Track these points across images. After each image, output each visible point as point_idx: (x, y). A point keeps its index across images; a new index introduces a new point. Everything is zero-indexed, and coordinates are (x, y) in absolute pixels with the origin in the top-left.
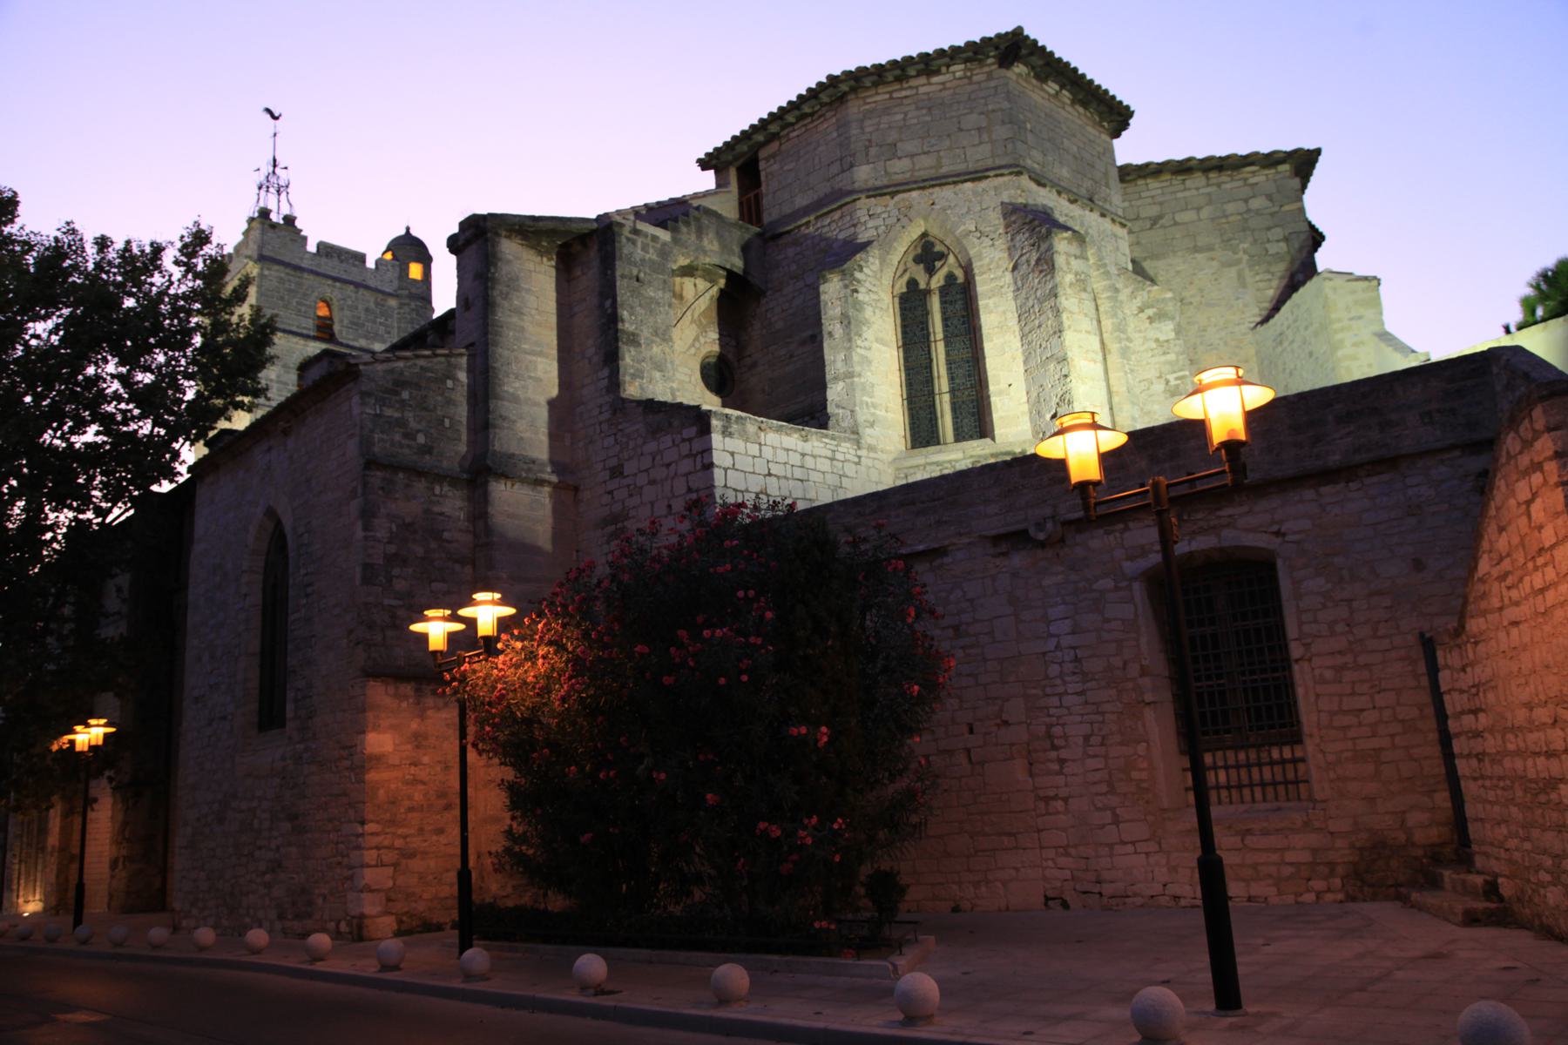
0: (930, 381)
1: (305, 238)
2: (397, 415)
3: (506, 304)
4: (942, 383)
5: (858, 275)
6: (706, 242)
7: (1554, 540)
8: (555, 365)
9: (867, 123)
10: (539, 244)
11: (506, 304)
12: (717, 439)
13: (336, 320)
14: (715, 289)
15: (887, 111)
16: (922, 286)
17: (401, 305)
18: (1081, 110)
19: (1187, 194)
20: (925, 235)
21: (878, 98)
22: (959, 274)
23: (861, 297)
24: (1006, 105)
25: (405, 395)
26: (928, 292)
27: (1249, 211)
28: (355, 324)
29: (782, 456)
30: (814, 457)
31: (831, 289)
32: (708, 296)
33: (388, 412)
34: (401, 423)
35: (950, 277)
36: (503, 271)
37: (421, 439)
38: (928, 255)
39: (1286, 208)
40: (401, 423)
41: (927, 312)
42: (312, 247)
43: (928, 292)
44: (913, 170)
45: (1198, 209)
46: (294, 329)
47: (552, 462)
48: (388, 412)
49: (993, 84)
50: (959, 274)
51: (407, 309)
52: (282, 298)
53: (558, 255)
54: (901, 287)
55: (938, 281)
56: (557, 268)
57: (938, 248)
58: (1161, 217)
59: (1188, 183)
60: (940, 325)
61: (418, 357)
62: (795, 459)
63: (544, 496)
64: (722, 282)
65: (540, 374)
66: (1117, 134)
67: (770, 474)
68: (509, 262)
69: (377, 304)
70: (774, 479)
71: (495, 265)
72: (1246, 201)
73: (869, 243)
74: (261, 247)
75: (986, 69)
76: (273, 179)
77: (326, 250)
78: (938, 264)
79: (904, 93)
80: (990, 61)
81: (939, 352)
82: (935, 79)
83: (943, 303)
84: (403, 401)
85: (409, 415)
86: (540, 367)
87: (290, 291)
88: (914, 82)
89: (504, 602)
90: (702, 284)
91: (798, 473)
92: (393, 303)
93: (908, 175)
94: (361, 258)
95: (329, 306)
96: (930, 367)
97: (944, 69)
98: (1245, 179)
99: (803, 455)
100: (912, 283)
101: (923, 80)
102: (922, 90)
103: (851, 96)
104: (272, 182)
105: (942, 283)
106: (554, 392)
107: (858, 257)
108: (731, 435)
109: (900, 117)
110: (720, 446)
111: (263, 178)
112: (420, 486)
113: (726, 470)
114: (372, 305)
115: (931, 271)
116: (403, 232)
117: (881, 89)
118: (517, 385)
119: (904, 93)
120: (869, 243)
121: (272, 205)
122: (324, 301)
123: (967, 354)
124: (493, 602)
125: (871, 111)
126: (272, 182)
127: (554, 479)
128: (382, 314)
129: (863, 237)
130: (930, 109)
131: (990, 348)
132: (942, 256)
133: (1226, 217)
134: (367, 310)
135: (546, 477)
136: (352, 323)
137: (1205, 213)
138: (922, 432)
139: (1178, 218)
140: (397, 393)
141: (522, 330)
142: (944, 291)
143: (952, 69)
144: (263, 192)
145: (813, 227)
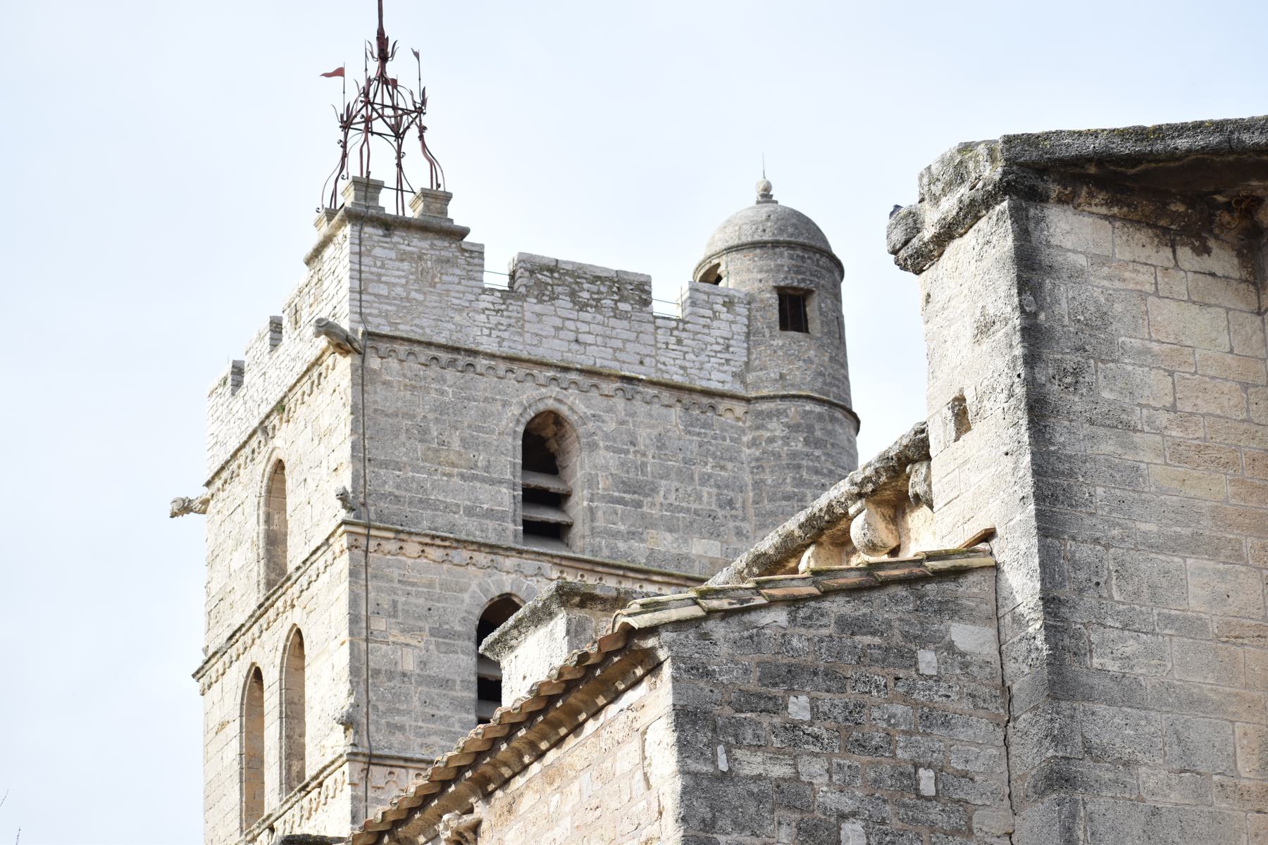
1: (477, 253)
2: (780, 770)
3: (1077, 403)
7: (990, 632)
11: (1077, 403)
25: (798, 708)
28: (634, 490)
33: (752, 764)
34: (790, 795)
40: (790, 795)
42: (496, 275)
48: (752, 764)
59: (591, 363)
66: (647, 303)
68: (1077, 275)
76: (381, 96)
77: (540, 278)
84: (795, 726)
85: (814, 769)
94: (635, 291)
104: (382, 107)
111: (353, 95)
121: (383, 170)
126: (382, 107)
136: (627, 486)
140: (777, 707)
144: (355, 138)
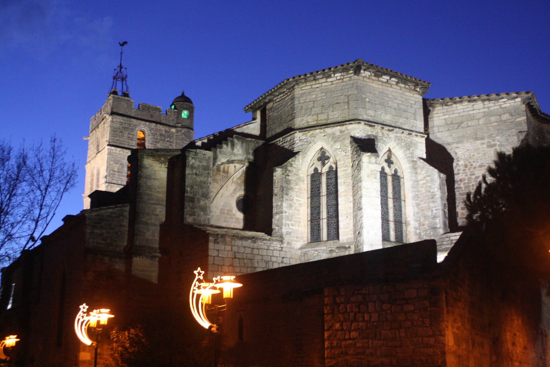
0: (394, 188)
4: (324, 214)
5: (289, 168)
6: (235, 151)
8: (165, 208)
9: (302, 99)
10: (160, 159)
12: (211, 245)
13: (147, 140)
14: (245, 168)
15: (309, 93)
16: (319, 171)
17: (177, 131)
18: (403, 85)
19: (474, 112)
20: (322, 148)
21: (307, 88)
22: (334, 166)
23: (290, 178)
24: (356, 92)
26: (321, 174)
27: (501, 121)
29: (242, 250)
30: (258, 249)
31: (278, 173)
32: (241, 171)
35: (331, 167)
36: (146, 172)
37: (108, 241)
38: (323, 158)
39: (517, 120)
41: (320, 183)
43: (321, 174)
44: (317, 120)
45: (479, 119)
46: (126, 146)
47: (160, 248)
49: (351, 82)
50: (334, 166)
51: (180, 133)
52: (121, 132)
53: (169, 162)
54: (311, 171)
55: (325, 169)
56: (168, 168)
57: (327, 154)
58: (462, 123)
59: (475, 107)
60: (325, 188)
61: (108, 208)
62: (248, 251)
63: (156, 263)
64: (247, 164)
65: (157, 212)
67: (235, 258)
69: (166, 131)
70: (237, 260)
71: (141, 170)
72: (500, 116)
73: (298, 152)
74: (112, 108)
75: (349, 76)
78: (326, 161)
79: (317, 86)
80: (351, 72)
81: (324, 200)
82: (329, 80)
83: (327, 179)
86: (158, 210)
87: (125, 128)
88: (321, 81)
89: (17, 338)
90: (238, 166)
91: (249, 256)
92: (173, 130)
93: (315, 122)
95: (144, 133)
96: (319, 207)
97: (333, 75)
98: (501, 105)
99: (253, 249)
100: (316, 169)
101: (324, 80)
102: (324, 84)
103: (296, 87)
105: (327, 170)
106: (164, 219)
107: (290, 160)
108: (218, 243)
109: (314, 96)
110: (213, 248)
112: (106, 259)
113: (214, 257)
114: (164, 133)
115: (324, 164)
116: (180, 94)
117: (308, 84)
118: (147, 218)
119: (317, 86)
120: (298, 152)
122: (141, 131)
123: (334, 202)
124: (230, 281)
125: (303, 94)
127: (159, 255)
128: (168, 136)
129: (296, 150)
130: (326, 93)
131: (246, 235)
132: (328, 158)
133: (491, 123)
134: (161, 135)
135: (157, 254)
137: (481, 122)
138: (315, 237)
139: (469, 123)
141: (151, 195)
142: (328, 173)
143: (336, 75)
145: (280, 142)
